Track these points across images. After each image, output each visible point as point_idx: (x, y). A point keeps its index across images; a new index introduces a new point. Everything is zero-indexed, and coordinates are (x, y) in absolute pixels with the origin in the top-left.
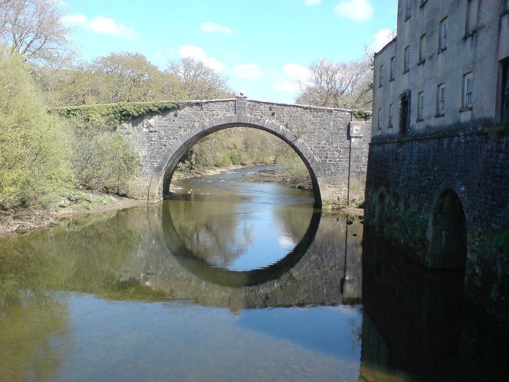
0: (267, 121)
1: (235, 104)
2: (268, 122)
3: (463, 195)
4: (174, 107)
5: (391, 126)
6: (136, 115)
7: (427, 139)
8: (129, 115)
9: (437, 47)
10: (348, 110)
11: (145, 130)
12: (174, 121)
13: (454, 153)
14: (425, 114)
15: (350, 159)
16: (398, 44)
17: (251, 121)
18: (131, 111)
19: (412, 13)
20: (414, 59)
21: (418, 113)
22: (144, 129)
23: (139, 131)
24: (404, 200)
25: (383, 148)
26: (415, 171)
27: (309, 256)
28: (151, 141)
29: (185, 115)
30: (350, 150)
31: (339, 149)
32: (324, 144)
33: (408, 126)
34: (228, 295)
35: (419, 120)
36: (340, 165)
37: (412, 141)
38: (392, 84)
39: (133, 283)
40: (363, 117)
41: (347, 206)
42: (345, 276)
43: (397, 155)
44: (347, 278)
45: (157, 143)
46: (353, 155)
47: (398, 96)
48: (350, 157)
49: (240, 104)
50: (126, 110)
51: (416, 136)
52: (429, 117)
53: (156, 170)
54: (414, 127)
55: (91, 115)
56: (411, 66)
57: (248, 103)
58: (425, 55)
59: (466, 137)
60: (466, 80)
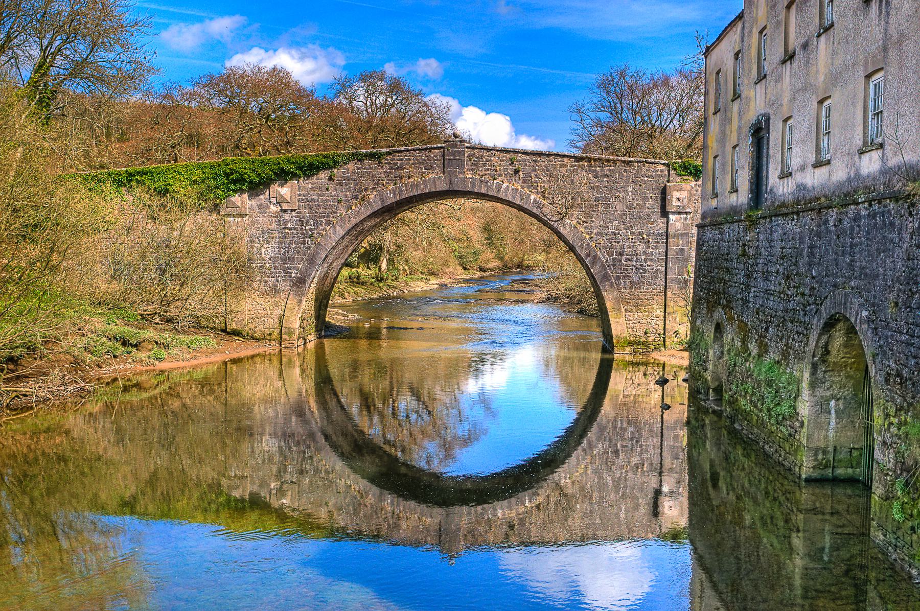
0: (505, 185)
1: (443, 156)
2: (507, 187)
3: (865, 326)
5: (735, 190)
7: (798, 213)
8: (241, 180)
9: (818, 24)
10: (663, 162)
11: (273, 208)
12: (327, 189)
13: (848, 240)
14: (796, 161)
15: (666, 256)
16: (747, 26)
17: (473, 185)
18: (246, 173)
20: (775, 53)
21: (782, 162)
22: (272, 206)
24: (756, 337)
26: (776, 277)
27: (591, 446)
28: (284, 229)
30: (667, 239)
31: (645, 236)
32: (617, 228)
33: (764, 187)
34: (437, 521)
35: (785, 175)
36: (647, 267)
37: (771, 217)
38: (736, 106)
39: (256, 503)
40: (691, 174)
41: (663, 349)
42: (661, 486)
43: (744, 245)
44: (665, 489)
47: (746, 130)
48: (666, 253)
50: (237, 172)
52: (803, 168)
53: (295, 285)
55: (171, 181)
56: (767, 67)
57: (468, 152)
59: (870, 205)
60: (872, 86)
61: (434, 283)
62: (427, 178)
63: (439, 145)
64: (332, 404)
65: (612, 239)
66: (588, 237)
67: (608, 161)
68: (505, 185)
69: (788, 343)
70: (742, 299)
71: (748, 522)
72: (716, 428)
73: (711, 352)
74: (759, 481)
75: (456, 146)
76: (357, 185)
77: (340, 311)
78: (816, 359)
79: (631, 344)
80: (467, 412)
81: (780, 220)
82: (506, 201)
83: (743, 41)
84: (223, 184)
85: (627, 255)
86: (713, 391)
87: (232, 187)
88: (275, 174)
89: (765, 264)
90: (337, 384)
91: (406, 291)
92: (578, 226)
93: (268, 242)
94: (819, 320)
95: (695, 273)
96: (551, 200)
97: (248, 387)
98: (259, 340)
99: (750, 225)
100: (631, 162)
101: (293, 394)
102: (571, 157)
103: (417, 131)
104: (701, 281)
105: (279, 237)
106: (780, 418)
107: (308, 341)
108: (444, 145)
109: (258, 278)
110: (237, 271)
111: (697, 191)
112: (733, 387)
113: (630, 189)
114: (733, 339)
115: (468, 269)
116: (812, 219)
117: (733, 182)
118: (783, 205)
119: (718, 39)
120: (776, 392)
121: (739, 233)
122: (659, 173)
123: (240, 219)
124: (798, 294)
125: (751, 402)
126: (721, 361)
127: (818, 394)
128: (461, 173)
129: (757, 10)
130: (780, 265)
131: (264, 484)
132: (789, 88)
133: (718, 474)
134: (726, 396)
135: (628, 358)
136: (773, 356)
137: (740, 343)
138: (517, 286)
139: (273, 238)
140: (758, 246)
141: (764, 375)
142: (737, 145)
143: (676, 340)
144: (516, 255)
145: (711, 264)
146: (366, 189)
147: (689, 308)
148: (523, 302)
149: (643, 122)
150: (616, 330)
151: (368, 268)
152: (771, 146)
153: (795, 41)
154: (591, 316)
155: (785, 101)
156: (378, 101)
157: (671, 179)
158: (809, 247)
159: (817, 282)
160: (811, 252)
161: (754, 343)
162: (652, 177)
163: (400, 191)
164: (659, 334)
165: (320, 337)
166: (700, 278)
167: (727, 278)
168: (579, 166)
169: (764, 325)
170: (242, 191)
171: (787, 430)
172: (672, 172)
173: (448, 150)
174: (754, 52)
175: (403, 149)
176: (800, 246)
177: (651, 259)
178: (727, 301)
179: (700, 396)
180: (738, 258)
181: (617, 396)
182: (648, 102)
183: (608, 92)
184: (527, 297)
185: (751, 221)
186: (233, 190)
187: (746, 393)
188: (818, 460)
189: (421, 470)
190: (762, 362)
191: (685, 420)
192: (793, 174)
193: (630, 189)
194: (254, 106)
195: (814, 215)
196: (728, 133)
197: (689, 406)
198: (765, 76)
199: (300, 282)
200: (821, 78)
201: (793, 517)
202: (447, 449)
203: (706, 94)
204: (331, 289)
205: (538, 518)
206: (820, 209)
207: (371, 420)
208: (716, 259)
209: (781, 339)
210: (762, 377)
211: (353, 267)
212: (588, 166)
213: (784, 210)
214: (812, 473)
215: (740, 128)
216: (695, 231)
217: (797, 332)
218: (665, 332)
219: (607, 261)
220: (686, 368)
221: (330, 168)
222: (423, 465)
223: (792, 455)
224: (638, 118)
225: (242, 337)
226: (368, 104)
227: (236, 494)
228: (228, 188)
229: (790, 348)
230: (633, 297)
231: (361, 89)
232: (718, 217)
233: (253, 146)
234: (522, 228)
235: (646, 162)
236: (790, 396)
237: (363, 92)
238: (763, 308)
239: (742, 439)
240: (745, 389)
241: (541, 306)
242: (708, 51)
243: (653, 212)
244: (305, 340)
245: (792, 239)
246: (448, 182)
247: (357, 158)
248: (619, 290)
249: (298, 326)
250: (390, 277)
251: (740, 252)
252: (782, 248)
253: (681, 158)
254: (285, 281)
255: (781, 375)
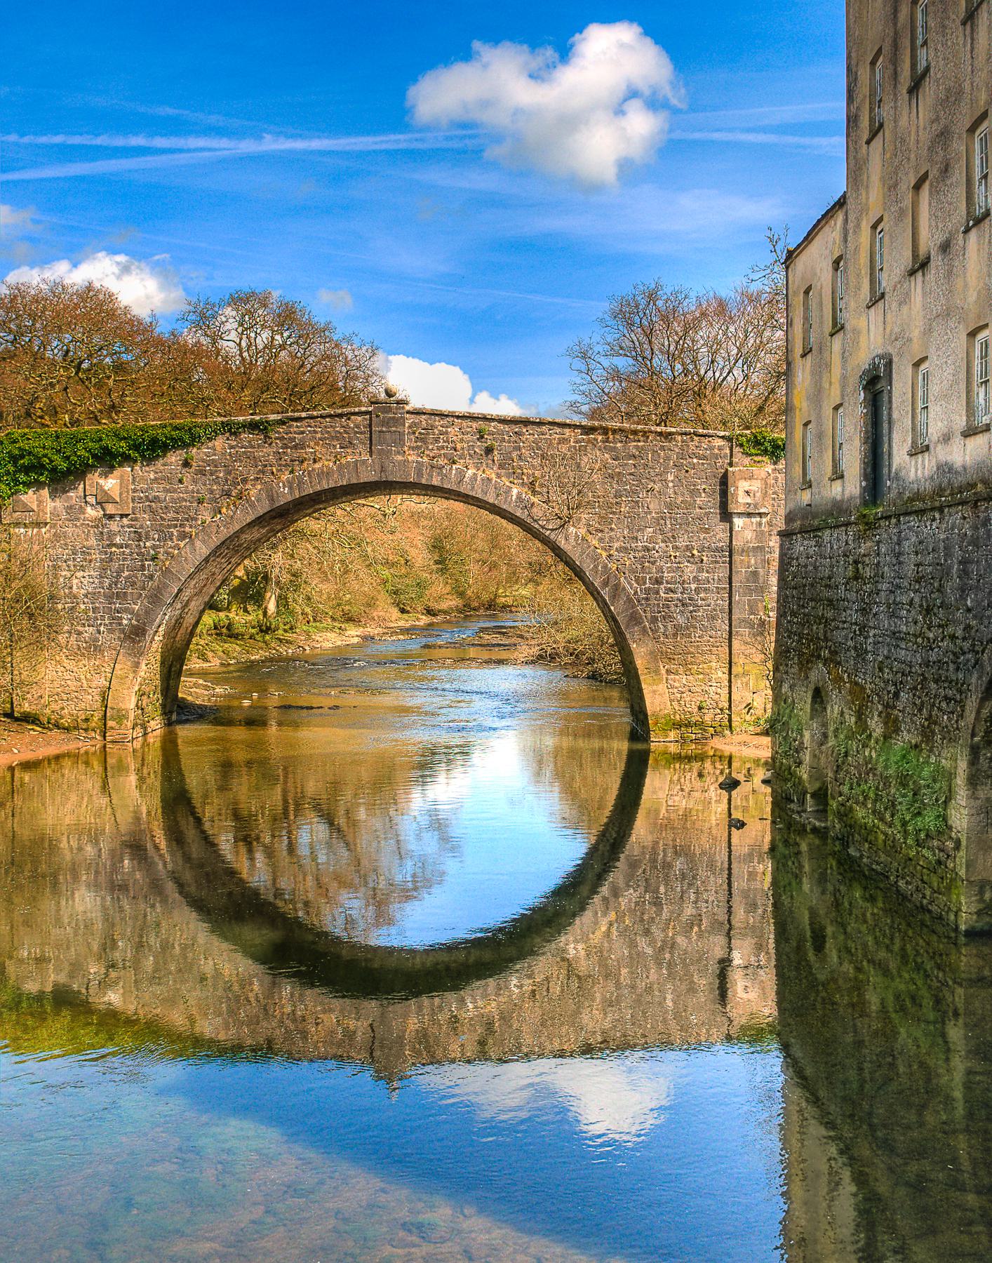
0: (470, 472)
4: (181, 439)
5: (838, 476)
6: (64, 466)
7: (941, 510)
8: (38, 467)
9: (964, 213)
10: (722, 434)
12: (181, 481)
14: (935, 429)
15: (730, 583)
16: (852, 217)
17: (420, 474)
18: (45, 456)
19: (886, 112)
20: (897, 260)
22: (89, 509)
23: (74, 513)
25: (819, 545)
26: (909, 611)
27: (616, 893)
29: (215, 464)
30: (730, 556)
31: (695, 552)
32: (651, 540)
33: (885, 471)
35: (920, 449)
36: (700, 602)
37: (898, 516)
38: (837, 343)
40: (766, 451)
41: (727, 732)
43: (856, 562)
44: (737, 959)
45: (128, 551)
46: (741, 572)
47: (854, 380)
48: (730, 578)
49: (383, 423)
50: (30, 453)
51: (911, 500)
52: (946, 438)
54: (903, 474)
56: (887, 281)
58: (929, 240)
61: (353, 634)
62: (343, 461)
63: (363, 409)
64: (191, 833)
65: (643, 557)
66: (604, 554)
67: (635, 432)
68: (470, 472)
69: (931, 716)
70: (855, 648)
71: (874, 1007)
72: (818, 854)
73: (807, 735)
74: (892, 939)
75: (389, 410)
76: (230, 473)
77: (201, 682)
78: (976, 739)
79: (677, 725)
80: (412, 845)
81: (913, 521)
82: (473, 498)
83: (845, 240)
84: (8, 473)
85: (668, 583)
86: (811, 797)
87: (22, 478)
88: (94, 456)
89: (892, 592)
90: (197, 801)
91: (307, 648)
92: (589, 537)
93: (83, 568)
94: (980, 678)
95: (778, 609)
96: (545, 494)
97: (50, 810)
98: (67, 729)
99: (865, 530)
100: (671, 434)
101: (125, 819)
102: (576, 427)
103: (324, 388)
104: (789, 622)
105: (102, 560)
106: (922, 835)
107: (150, 730)
108: (370, 409)
109: (66, 628)
110: (31, 616)
111: (776, 479)
112: (845, 789)
113: (670, 478)
114: (842, 713)
115: (408, 612)
116: (964, 518)
117: (836, 463)
118: (918, 496)
119: (806, 238)
120: (915, 794)
121: (847, 543)
122: (716, 451)
123: (35, 530)
124: (945, 637)
125: (874, 812)
126: (823, 747)
127: (981, 794)
128: (399, 453)
129: (867, 193)
130: (916, 591)
131: (76, 968)
132: (921, 314)
133: (823, 929)
134: (834, 804)
135: (673, 748)
136: (907, 737)
137: (853, 719)
138: (487, 637)
139: (91, 561)
140: (879, 562)
141: (894, 767)
142: (841, 405)
143: (748, 718)
144: (485, 587)
145: (804, 593)
146: (245, 481)
147: (770, 665)
148: (500, 662)
149: (686, 372)
150: (652, 703)
151: (246, 611)
152: (894, 406)
153: (929, 240)
154: (610, 682)
155: (916, 334)
156: (259, 340)
157: (735, 460)
158: (960, 562)
159: (975, 617)
160: (964, 570)
161: (876, 718)
162: (705, 458)
163: (301, 483)
164: (721, 710)
165: (169, 724)
166: (786, 617)
167: (829, 614)
168: (589, 441)
169: (892, 689)
170: (39, 485)
171: (934, 855)
172: (736, 450)
173: (378, 416)
174: (864, 259)
175: (304, 415)
176: (946, 560)
177: (705, 589)
178: (830, 652)
179: (792, 806)
180: (847, 583)
181: (657, 811)
182: (693, 341)
183: (630, 325)
184: (504, 655)
185: (867, 524)
186: (24, 483)
187: (866, 798)
188: (984, 901)
189: (337, 941)
190: (890, 747)
191: (766, 847)
192: (932, 447)
193: (670, 478)
194: (54, 351)
195: (968, 512)
196: (826, 385)
197: (773, 822)
198: (883, 296)
199: (136, 634)
200: (972, 296)
201: (947, 995)
202: (381, 905)
203: (790, 323)
204: (189, 642)
205: (531, 1013)
206: (976, 502)
207: (252, 859)
208: (812, 585)
209: (920, 710)
210: (891, 772)
211: (219, 610)
212: (603, 442)
213: (919, 505)
214: (977, 922)
215: (844, 378)
216: (774, 542)
217: (946, 698)
218: (730, 706)
219: (636, 593)
220: (766, 763)
221: (186, 445)
222: (338, 930)
223: (944, 895)
224: (678, 367)
225: (41, 725)
226: (244, 344)
227: (32, 987)
228: (16, 481)
229: (935, 723)
230: (679, 650)
231: (231, 320)
232: (813, 518)
233: (54, 412)
234: (494, 544)
235: (696, 434)
236: (937, 800)
237: (235, 325)
238: (889, 661)
239: (862, 872)
240: (863, 792)
241: (528, 670)
242: (791, 256)
243: (707, 514)
244: (145, 728)
245: (933, 550)
246: (377, 467)
247: (230, 430)
248: (656, 639)
249: (132, 705)
250: (281, 625)
251: (850, 573)
252: (917, 565)
253: (747, 428)
254: (111, 631)
255: (920, 767)
